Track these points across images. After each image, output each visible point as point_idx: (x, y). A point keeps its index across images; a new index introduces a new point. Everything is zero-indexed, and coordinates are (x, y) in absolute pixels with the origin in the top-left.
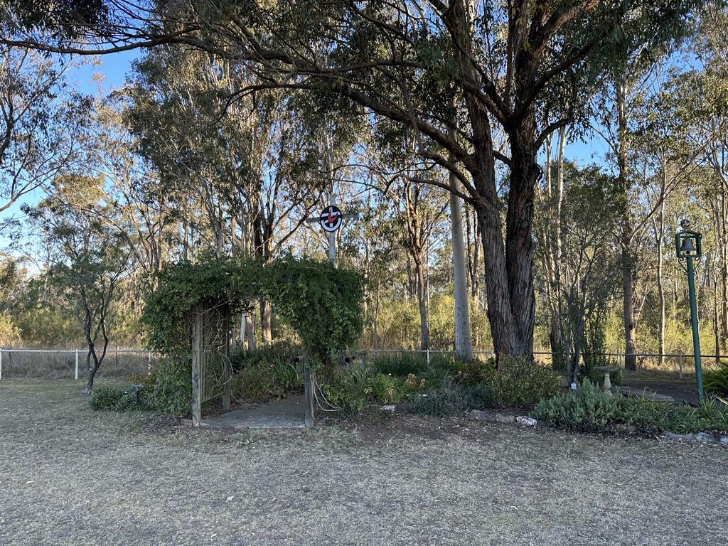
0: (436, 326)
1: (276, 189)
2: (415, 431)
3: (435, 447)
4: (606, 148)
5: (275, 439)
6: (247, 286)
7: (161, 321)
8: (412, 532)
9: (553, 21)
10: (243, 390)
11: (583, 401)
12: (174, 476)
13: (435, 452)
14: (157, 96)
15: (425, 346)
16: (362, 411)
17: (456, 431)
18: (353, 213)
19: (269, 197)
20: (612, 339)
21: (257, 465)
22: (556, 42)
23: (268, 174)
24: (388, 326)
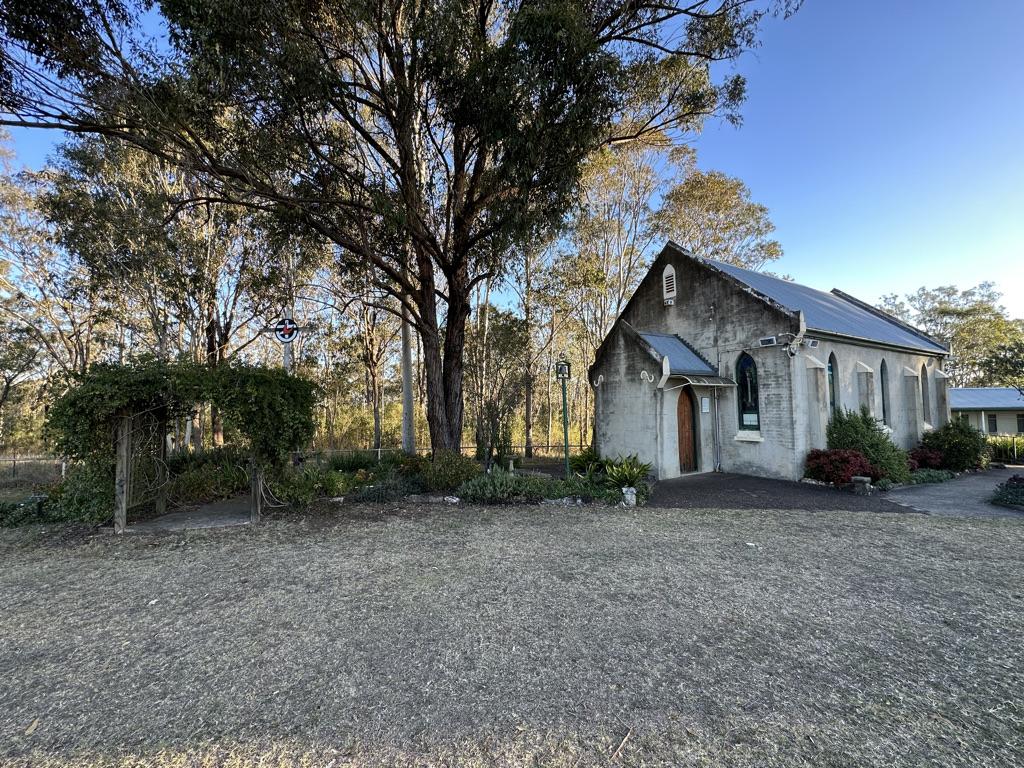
0: (388, 429)
1: (235, 299)
2: (360, 517)
3: (376, 528)
4: (517, 299)
5: (217, 537)
6: (187, 390)
7: (75, 425)
8: (346, 602)
9: (482, 198)
10: (178, 493)
11: (493, 481)
12: (80, 589)
13: (376, 532)
14: (91, 189)
15: (377, 446)
16: (311, 504)
17: (395, 514)
18: (312, 327)
19: (226, 306)
20: (517, 437)
21: (192, 565)
22: (483, 214)
23: (225, 285)
24: (345, 429)
